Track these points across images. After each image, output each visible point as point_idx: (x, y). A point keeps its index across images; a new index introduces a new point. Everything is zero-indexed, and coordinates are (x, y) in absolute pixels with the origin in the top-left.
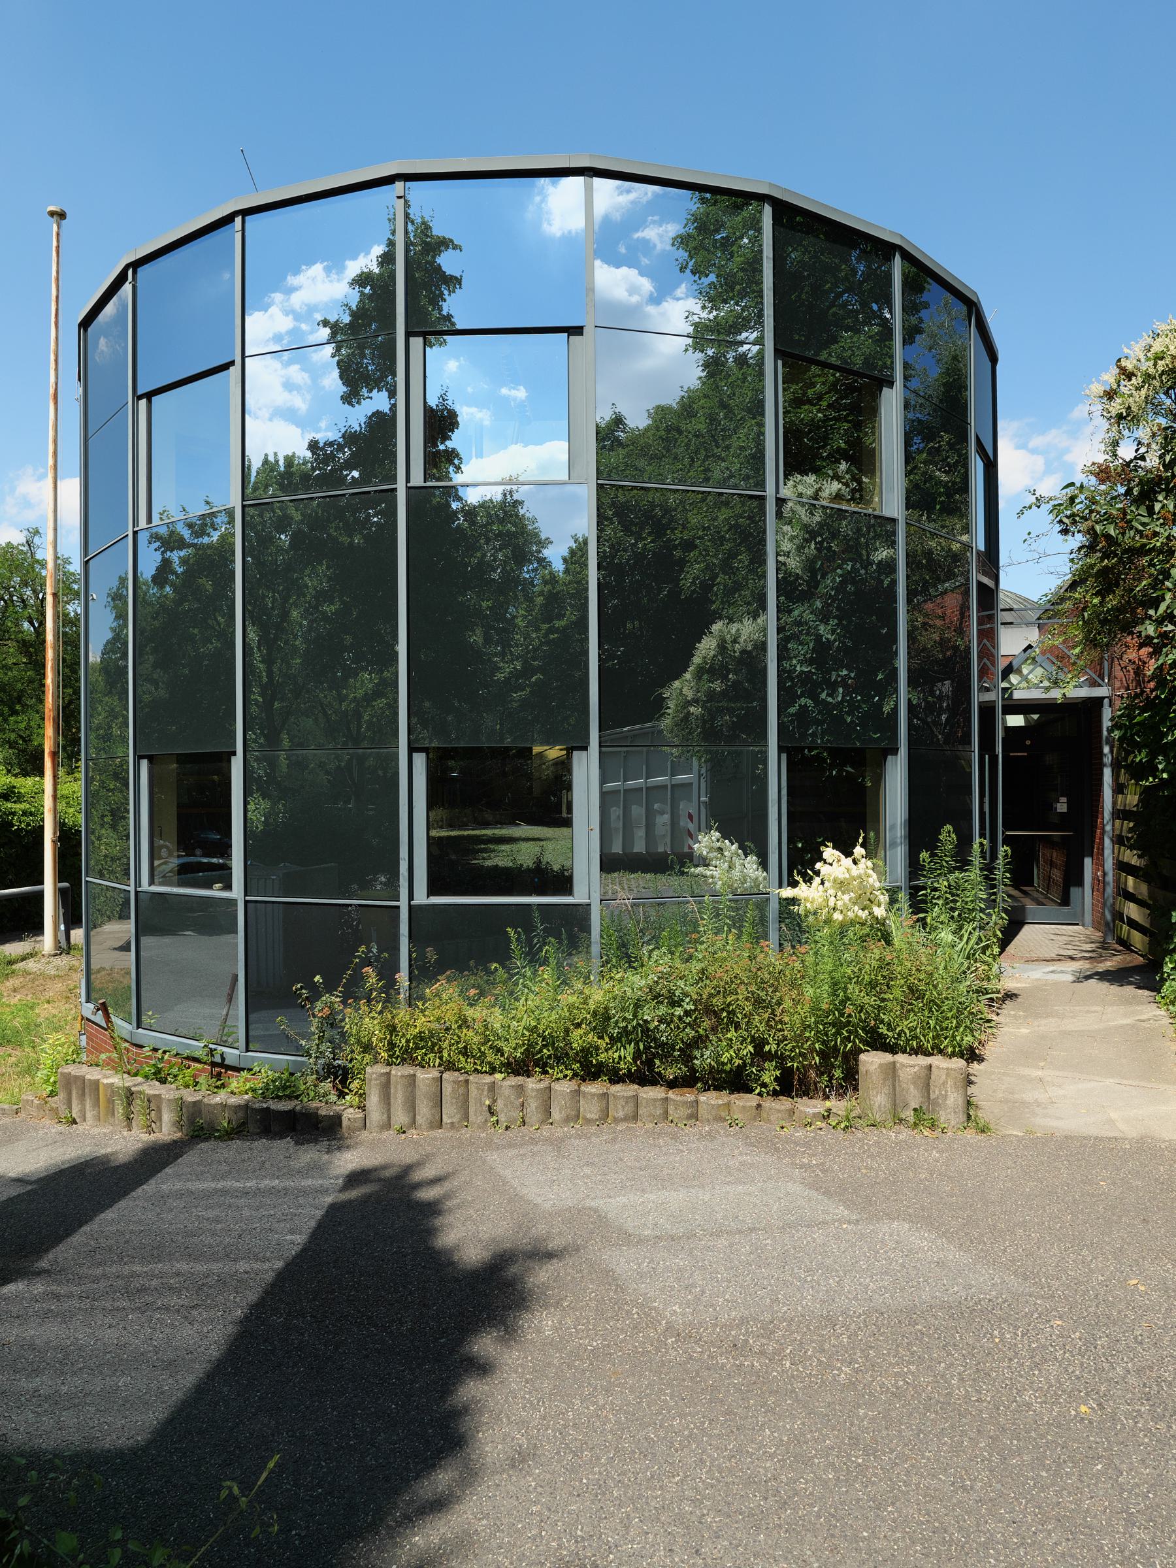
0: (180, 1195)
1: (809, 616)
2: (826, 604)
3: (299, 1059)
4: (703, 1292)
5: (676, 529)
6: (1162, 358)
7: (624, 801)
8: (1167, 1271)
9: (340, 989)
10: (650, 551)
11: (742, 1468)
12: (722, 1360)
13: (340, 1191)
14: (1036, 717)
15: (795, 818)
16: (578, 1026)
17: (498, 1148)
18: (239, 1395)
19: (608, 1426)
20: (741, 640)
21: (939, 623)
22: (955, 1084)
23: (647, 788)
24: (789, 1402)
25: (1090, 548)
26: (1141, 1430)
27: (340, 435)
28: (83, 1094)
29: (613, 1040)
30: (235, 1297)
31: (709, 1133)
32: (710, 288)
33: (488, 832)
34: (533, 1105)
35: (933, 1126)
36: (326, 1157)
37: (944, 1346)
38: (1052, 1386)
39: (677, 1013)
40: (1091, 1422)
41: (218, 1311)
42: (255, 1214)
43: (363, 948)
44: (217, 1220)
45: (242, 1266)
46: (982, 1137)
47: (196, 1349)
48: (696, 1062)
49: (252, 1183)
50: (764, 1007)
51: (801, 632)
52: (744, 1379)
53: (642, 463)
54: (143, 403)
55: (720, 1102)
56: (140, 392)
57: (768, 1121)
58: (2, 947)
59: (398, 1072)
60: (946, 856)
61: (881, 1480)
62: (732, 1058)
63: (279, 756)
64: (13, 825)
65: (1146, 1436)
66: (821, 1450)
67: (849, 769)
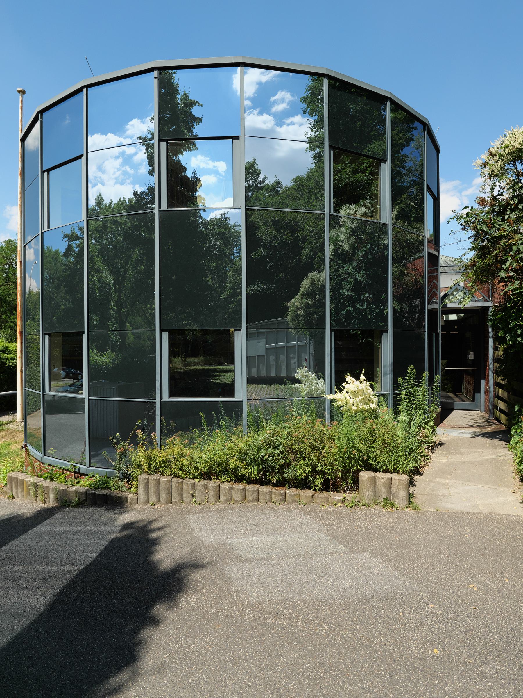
0: (49, 533)
1: (351, 269)
2: (358, 264)
3: (112, 470)
4: (269, 586)
5: (300, 231)
6: (508, 147)
7: (276, 352)
8: (489, 580)
9: (129, 439)
10: (289, 240)
11: (265, 677)
12: (269, 621)
13: (119, 532)
14: (462, 315)
15: (338, 361)
16: (233, 457)
17: (194, 513)
18: (46, 632)
19: (208, 653)
20: (321, 280)
21: (414, 273)
22: (403, 487)
23: (287, 347)
24: (295, 643)
25: (476, 237)
26: (461, 663)
27: (147, 188)
28: (17, 485)
29: (248, 465)
30: (58, 583)
31: (290, 508)
32: (315, 122)
33: (221, 367)
34: (211, 494)
35: (392, 506)
36: (117, 516)
37: (375, 616)
38: (422, 638)
39: (276, 452)
40: (437, 658)
41: (49, 590)
42: (79, 543)
43: (140, 421)
44: (61, 546)
45: (66, 568)
46: (414, 512)
47: (34, 608)
48: (285, 475)
49: (82, 528)
50: (317, 450)
51: (348, 277)
52: (277, 631)
53: (288, 202)
54: (45, 174)
55: (295, 494)
56: (44, 169)
57: (317, 503)
58: (1, 418)
59: (152, 478)
60: (410, 379)
61: (330, 685)
62: (302, 473)
63: (127, 334)
64: (6, 364)
65: (463, 666)
66: (305, 668)
67: (370, 339)
